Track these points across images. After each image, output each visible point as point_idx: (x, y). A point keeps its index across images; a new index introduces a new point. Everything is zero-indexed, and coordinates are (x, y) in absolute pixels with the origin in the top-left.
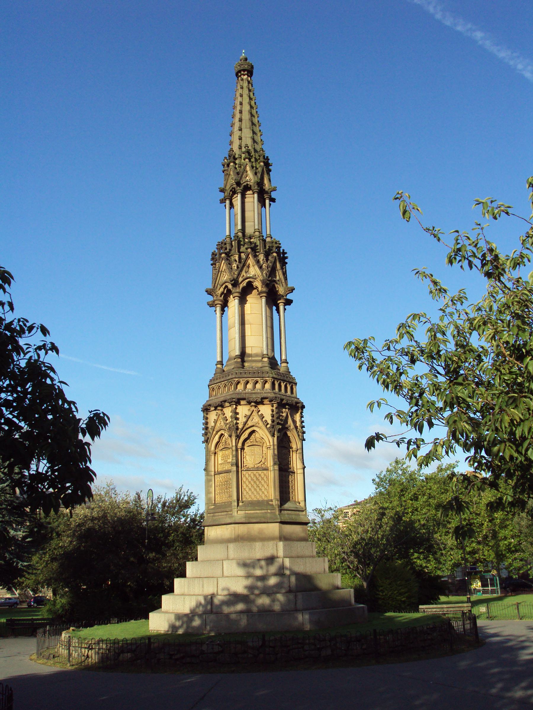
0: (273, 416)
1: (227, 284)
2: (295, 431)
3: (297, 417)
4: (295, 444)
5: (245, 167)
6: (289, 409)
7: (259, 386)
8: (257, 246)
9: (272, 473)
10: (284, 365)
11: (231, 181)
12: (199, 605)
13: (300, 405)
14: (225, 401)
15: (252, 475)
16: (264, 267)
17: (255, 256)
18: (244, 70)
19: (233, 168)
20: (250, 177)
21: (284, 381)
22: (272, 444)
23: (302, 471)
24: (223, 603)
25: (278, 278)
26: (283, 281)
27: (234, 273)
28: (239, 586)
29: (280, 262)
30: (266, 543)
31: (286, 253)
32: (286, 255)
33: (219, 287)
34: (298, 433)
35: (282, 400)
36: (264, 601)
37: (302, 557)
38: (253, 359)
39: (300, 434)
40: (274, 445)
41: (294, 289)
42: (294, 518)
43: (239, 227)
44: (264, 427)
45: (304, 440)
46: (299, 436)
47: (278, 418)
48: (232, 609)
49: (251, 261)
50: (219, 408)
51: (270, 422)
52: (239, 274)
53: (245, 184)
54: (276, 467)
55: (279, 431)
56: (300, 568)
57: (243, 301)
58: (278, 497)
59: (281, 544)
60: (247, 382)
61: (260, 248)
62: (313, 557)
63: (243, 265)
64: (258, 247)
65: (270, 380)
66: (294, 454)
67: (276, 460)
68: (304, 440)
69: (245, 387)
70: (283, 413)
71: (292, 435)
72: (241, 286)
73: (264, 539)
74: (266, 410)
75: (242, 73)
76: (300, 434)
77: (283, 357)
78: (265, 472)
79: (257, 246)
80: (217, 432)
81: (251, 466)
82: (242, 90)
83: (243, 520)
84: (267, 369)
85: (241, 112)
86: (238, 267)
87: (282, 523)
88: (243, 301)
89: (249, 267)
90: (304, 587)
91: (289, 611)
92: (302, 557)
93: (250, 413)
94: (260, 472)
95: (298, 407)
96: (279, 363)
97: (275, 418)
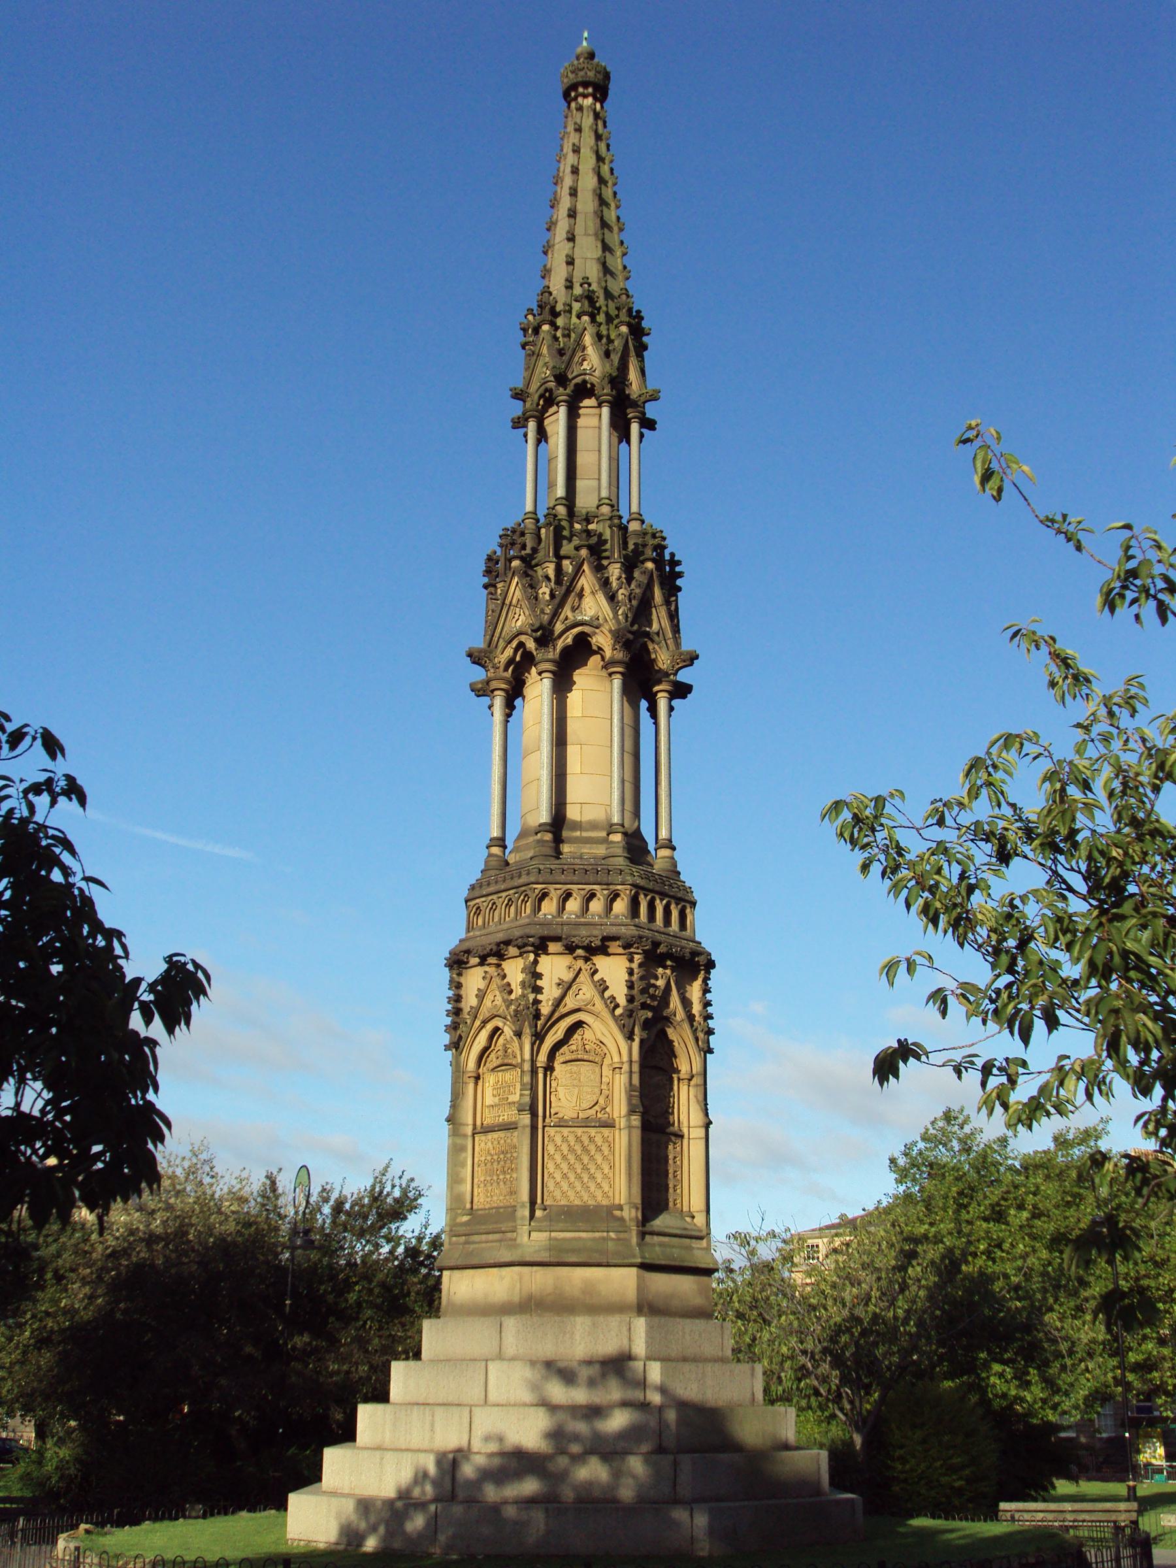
0: (631, 986)
1: (523, 638)
2: (686, 1026)
3: (695, 991)
6: (673, 969)
7: (596, 906)
8: (606, 541)
9: (625, 1134)
11: (544, 372)
13: (701, 959)
14: (507, 943)
15: (572, 1139)
16: (620, 597)
17: (599, 569)
18: (586, 85)
19: (548, 338)
20: (592, 363)
21: (663, 895)
22: (625, 1058)
23: (702, 1133)
27: (542, 611)
28: (529, 1432)
30: (601, 1319)
31: (678, 563)
32: (678, 569)
33: (502, 644)
34: (695, 1031)
35: (656, 944)
36: (593, 1471)
37: (695, 1360)
38: (585, 834)
39: (701, 1035)
40: (631, 1062)
41: (697, 657)
43: (560, 491)
45: (711, 1051)
46: (697, 1039)
47: (644, 991)
49: (587, 581)
51: (622, 1001)
52: (555, 614)
53: (579, 380)
54: (636, 1120)
55: (646, 1025)
56: (690, 1389)
57: (562, 684)
58: (638, 1200)
61: (613, 548)
62: (722, 1360)
63: (566, 590)
64: (608, 546)
65: (626, 892)
68: (711, 1051)
71: (680, 1036)
72: (560, 644)
73: (596, 1307)
74: (615, 970)
75: (581, 90)
76: (701, 1035)
77: (663, 834)
78: (606, 1131)
79: (606, 541)
80: (485, 1022)
82: (577, 135)
83: (544, 1256)
84: (621, 862)
86: (552, 596)
87: (647, 1267)
88: (562, 684)
89: (581, 595)
90: (695, 1438)
91: (654, 1502)
92: (695, 1360)
93: (571, 975)
94: (592, 1131)
96: (651, 847)
97: (635, 992)
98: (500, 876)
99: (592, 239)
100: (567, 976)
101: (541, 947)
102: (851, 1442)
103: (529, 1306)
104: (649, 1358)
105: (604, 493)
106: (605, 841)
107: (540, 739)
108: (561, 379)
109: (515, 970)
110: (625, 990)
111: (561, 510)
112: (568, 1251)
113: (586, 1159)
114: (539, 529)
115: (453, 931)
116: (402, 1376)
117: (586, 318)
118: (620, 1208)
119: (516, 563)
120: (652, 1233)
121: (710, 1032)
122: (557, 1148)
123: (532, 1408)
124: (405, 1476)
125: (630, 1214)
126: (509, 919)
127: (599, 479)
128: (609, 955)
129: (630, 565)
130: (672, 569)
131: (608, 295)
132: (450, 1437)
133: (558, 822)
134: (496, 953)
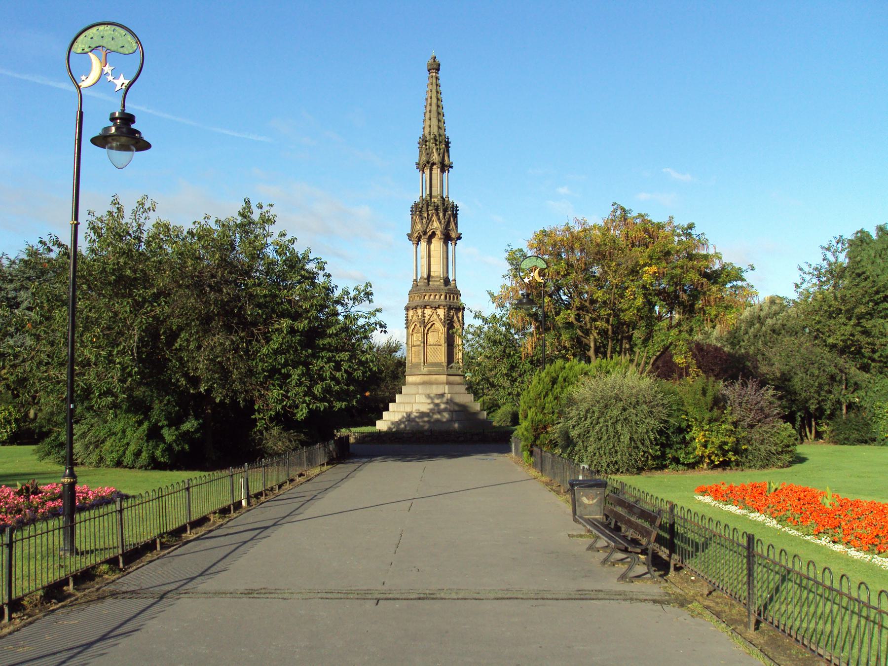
3: (460, 314)
11: (424, 158)
17: (437, 215)
20: (435, 157)
28: (425, 408)
36: (437, 416)
49: (434, 218)
57: (429, 242)
59: (447, 387)
63: (429, 220)
73: (437, 383)
74: (441, 312)
84: (443, 287)
85: (431, 105)
90: (461, 411)
91: (450, 421)
98: (416, 289)
101: (425, 307)
103: (424, 383)
108: (428, 162)
109: (419, 312)
115: (406, 301)
116: (398, 397)
124: (400, 417)
125: (445, 364)
126: (418, 301)
129: (445, 211)
131: (440, 135)
132: (409, 410)
133: (429, 276)
134: (416, 308)
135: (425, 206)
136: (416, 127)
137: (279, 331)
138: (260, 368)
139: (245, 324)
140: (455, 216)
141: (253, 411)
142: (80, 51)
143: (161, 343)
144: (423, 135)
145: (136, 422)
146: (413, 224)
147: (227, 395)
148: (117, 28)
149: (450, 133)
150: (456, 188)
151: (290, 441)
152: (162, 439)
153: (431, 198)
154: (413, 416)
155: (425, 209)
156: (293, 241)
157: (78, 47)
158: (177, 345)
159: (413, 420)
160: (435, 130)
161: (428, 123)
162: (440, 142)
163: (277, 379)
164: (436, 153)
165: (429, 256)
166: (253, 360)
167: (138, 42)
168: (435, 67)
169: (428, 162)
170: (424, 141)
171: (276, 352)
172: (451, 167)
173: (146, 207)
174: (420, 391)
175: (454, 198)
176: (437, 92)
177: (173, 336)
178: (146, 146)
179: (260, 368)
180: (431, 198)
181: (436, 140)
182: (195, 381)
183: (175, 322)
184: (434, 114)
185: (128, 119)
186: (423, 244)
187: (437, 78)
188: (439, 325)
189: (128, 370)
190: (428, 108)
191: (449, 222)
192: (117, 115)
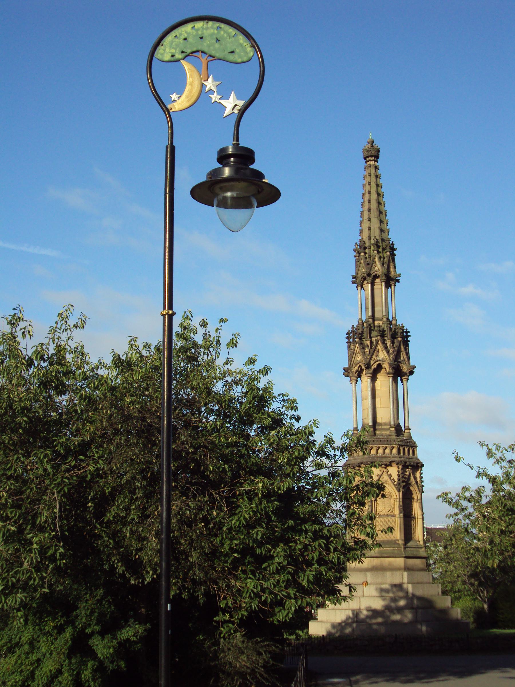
0: (399, 476)
1: (361, 364)
2: (416, 485)
3: (418, 474)
4: (416, 496)
5: (374, 259)
6: (411, 469)
7: (388, 451)
8: (385, 331)
9: (399, 519)
10: (407, 431)
11: (363, 270)
12: (348, 618)
13: (420, 465)
14: (362, 463)
15: (383, 521)
16: (391, 352)
17: (384, 342)
18: (371, 156)
19: (363, 258)
20: (378, 268)
21: (407, 446)
22: (398, 497)
23: (421, 517)
24: (367, 617)
25: (402, 358)
26: (406, 360)
27: (367, 358)
28: (378, 604)
29: (403, 345)
30: (394, 572)
31: (409, 332)
32: (408, 334)
33: (354, 365)
34: (418, 487)
35: (406, 463)
36: (397, 617)
37: (421, 583)
38: (383, 427)
39: (420, 488)
40: (400, 498)
41: (415, 367)
42: (415, 553)
43: (370, 314)
44: (392, 484)
45: (423, 492)
46: (419, 489)
47: (403, 477)
48: (374, 621)
49: (380, 347)
50: (357, 468)
51: (396, 480)
52: (371, 358)
53: (374, 274)
54: (402, 515)
55: (404, 487)
56: (419, 592)
57: (374, 379)
58: (403, 538)
59: (405, 574)
60: (379, 448)
61: (388, 334)
62: (429, 583)
63: (374, 350)
64: (386, 333)
65: (396, 447)
66: (415, 504)
67: (402, 510)
68: (423, 492)
69: (377, 452)
70: (406, 472)
71: (414, 489)
72: (373, 368)
73: (393, 569)
74: (394, 471)
76: (420, 488)
77: (407, 425)
78: (393, 518)
79: (385, 331)
81: (382, 513)
82: (370, 177)
83: (377, 555)
84: (394, 437)
85: (369, 201)
86: (369, 352)
87: (406, 557)
88: (374, 379)
89: (378, 351)
90: (423, 606)
91: (414, 622)
92: (421, 583)
93: (381, 473)
94: (389, 518)
95: (418, 466)
96: (403, 429)
97: (400, 478)
99: (376, 219)
100: (380, 473)
102: (483, 608)
104: (408, 583)
105: (384, 314)
106: (389, 429)
107: (367, 395)
108: (369, 275)
110: (397, 477)
111: (371, 320)
112: (383, 553)
113: (385, 523)
114: (363, 324)
117: (376, 252)
118: (398, 540)
119: (357, 340)
120: (408, 548)
121: (423, 486)
122: (379, 523)
123: (376, 598)
125: (401, 542)
127: (382, 307)
128: (392, 466)
129: (394, 337)
130: (407, 334)
131: (383, 240)
135: (366, 331)
136: (349, 231)
137: (251, 495)
138: (226, 546)
139: (206, 485)
140: (406, 342)
141: (217, 609)
142: (167, 57)
143: (90, 512)
144: (361, 241)
145: (55, 627)
146: (351, 355)
147: (184, 588)
148: (222, 25)
149: (393, 237)
150: (404, 307)
151: (260, 654)
152: (91, 653)
153: (374, 320)
154: (362, 616)
155: (366, 334)
156: (266, 371)
157: (165, 52)
158: (109, 516)
159: (363, 621)
160: (376, 233)
161: (366, 224)
162: (384, 249)
163: (249, 563)
164: (377, 263)
165: (374, 397)
166: (216, 536)
167: (255, 45)
168: (373, 154)
169: (369, 275)
170: (361, 248)
171: (250, 526)
172: (398, 281)
173: (71, 322)
174: (369, 580)
175: (403, 320)
176: (378, 185)
177: (104, 502)
178: (269, 195)
179: (226, 546)
180: (374, 320)
181: (378, 247)
182: (135, 567)
183: (107, 485)
184: (374, 213)
185: (245, 156)
186: (366, 381)
187: (376, 168)
188: (390, 489)
189: (50, 552)
190: (366, 207)
191: (399, 352)
192: (230, 150)
